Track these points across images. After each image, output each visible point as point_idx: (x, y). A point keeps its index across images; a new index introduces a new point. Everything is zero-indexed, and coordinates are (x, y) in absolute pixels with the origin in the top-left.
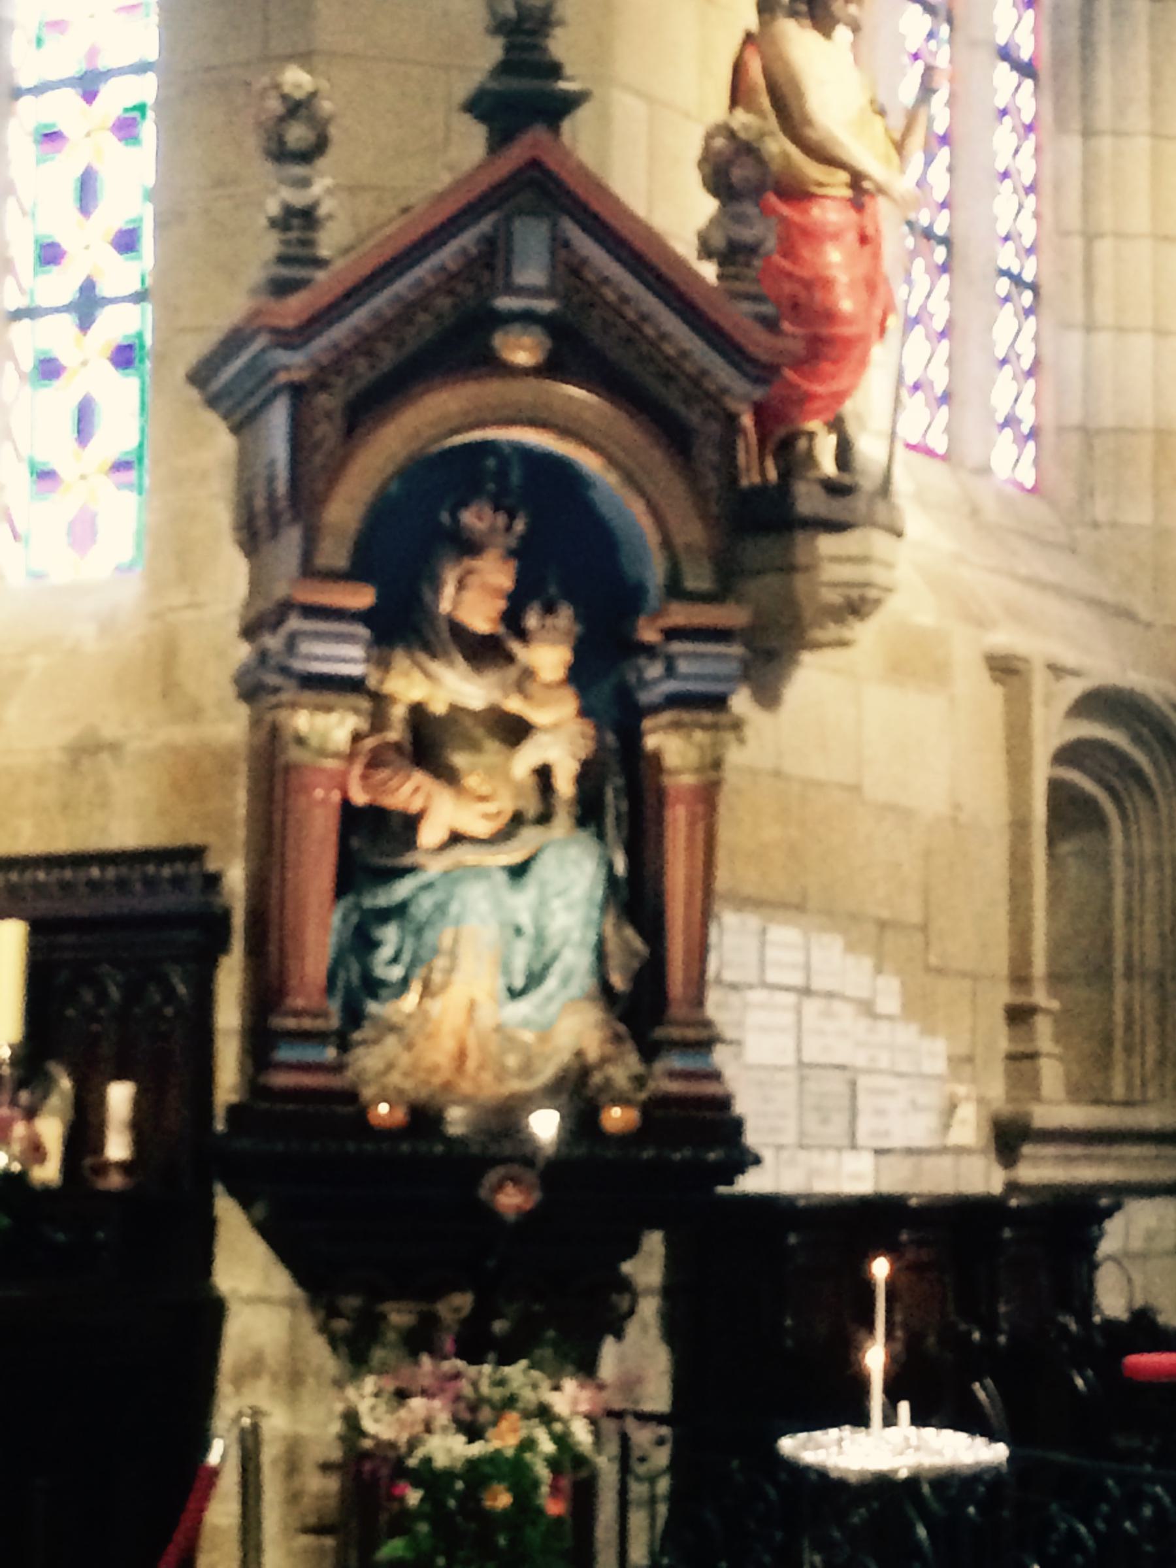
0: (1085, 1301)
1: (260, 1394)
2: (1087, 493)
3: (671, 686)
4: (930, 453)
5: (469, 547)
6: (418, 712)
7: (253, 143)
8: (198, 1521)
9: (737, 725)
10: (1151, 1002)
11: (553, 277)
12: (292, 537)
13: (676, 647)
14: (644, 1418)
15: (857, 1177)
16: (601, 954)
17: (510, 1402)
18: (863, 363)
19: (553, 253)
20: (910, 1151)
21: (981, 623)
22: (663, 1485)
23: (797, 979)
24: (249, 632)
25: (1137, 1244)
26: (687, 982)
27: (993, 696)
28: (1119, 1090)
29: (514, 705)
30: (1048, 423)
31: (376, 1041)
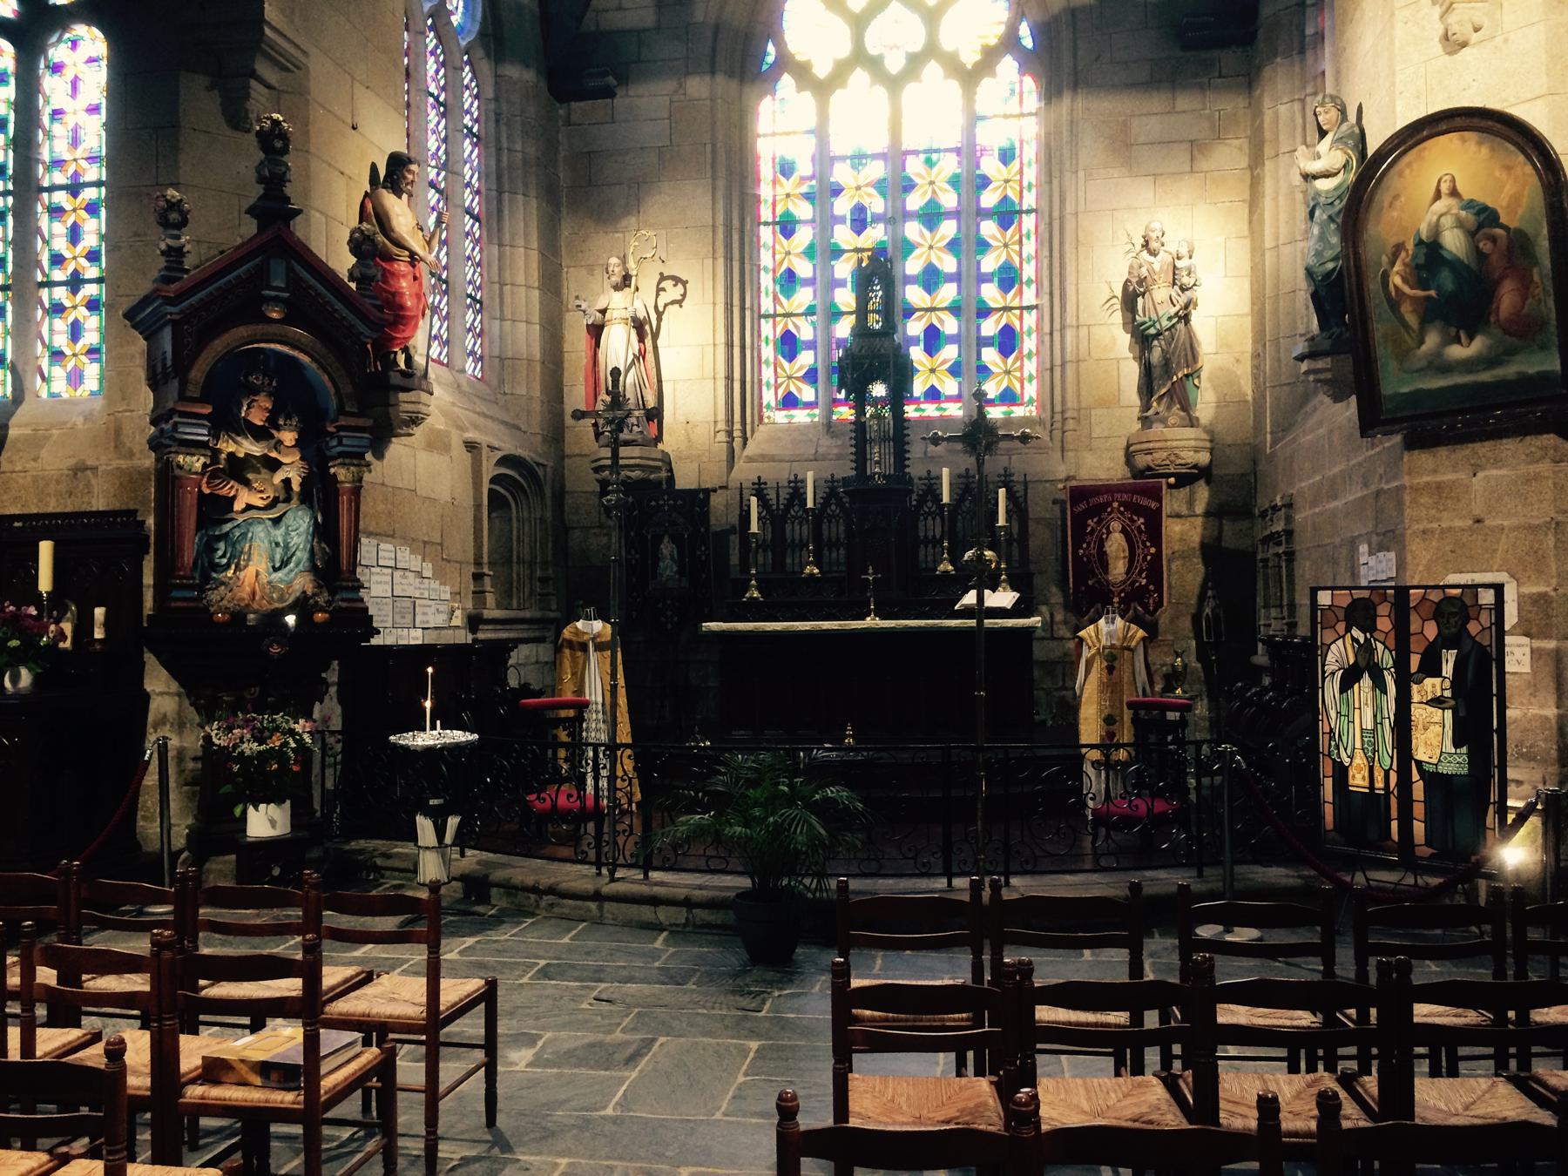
0: (504, 681)
1: (165, 731)
2: (502, 382)
3: (340, 449)
5: (254, 391)
6: (231, 455)
7: (152, 219)
8: (140, 783)
9: (368, 465)
10: (527, 572)
11: (287, 284)
12: (175, 384)
13: (342, 434)
14: (333, 733)
16: (312, 552)
17: (277, 729)
18: (416, 326)
19: (287, 275)
20: (436, 628)
21: (462, 429)
23: (392, 563)
24: (154, 422)
26: (348, 562)
28: (515, 606)
29: (274, 454)
31: (216, 588)
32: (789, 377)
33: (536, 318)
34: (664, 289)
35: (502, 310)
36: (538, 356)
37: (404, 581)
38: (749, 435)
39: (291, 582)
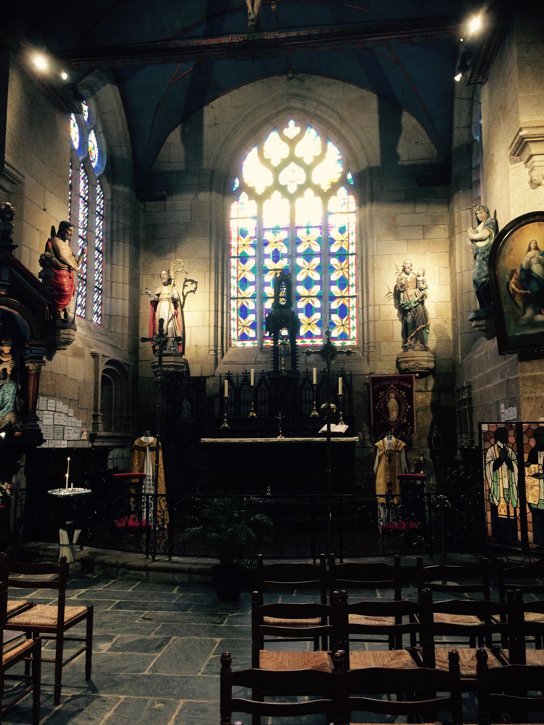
2: (110, 326)
3: (31, 355)
4: (82, 317)
9: (44, 362)
14: (21, 490)
15: (64, 445)
18: (70, 300)
21: (90, 347)
22: (24, 502)
25: (115, 457)
27: (92, 360)
30: (103, 314)
32: (244, 326)
33: (127, 297)
34: (186, 286)
35: (111, 294)
36: (127, 314)
37: (60, 418)
38: (225, 352)
39: (4, 417)
